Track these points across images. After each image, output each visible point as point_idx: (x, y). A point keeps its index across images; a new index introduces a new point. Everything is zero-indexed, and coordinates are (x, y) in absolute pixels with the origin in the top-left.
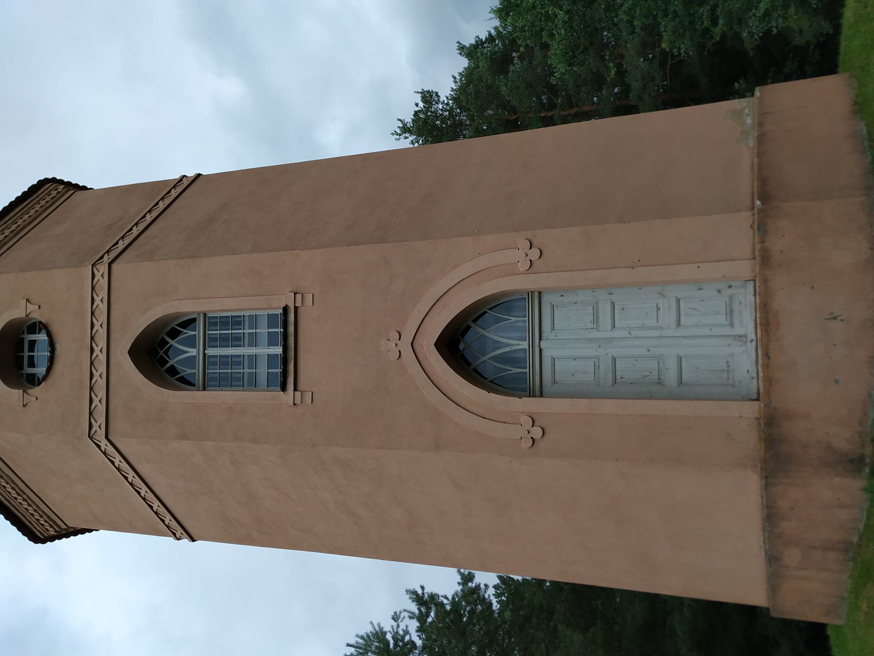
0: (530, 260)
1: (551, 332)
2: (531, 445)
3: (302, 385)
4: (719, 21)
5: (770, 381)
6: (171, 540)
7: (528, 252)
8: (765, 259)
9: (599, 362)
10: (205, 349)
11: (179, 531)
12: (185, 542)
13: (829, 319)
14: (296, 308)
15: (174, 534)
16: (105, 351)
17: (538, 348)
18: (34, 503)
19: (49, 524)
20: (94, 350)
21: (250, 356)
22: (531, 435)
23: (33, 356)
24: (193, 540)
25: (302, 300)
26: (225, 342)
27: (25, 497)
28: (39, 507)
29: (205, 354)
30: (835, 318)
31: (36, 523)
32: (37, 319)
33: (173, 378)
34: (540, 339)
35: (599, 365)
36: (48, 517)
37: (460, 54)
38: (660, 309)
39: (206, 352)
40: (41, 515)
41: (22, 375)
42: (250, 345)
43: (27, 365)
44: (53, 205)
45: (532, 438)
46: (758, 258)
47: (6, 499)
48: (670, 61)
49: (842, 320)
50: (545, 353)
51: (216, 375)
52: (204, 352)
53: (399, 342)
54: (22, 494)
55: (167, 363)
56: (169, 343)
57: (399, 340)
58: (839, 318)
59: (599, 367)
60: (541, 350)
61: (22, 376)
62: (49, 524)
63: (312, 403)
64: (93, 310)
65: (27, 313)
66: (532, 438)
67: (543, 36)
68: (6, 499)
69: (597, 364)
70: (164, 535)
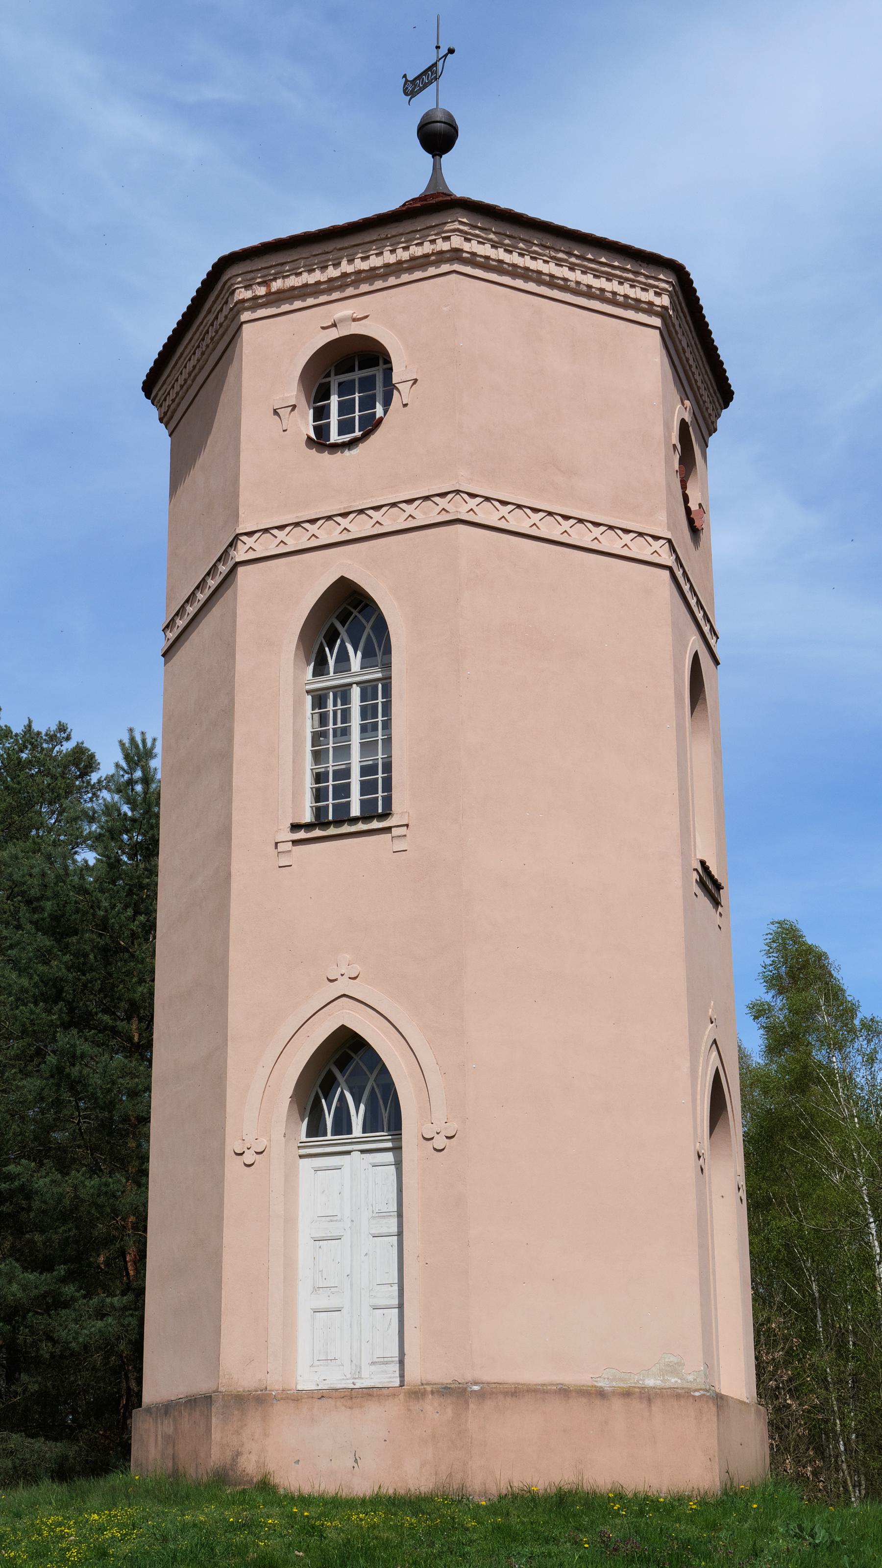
0: (433, 1138)
2: (236, 1152)
5: (298, 1400)
7: (442, 1134)
8: (417, 1394)
9: (336, 1221)
10: (357, 683)
13: (355, 1455)
14: (388, 830)
17: (351, 1149)
18: (186, 393)
20: (346, 518)
21: (348, 785)
22: (247, 1151)
23: (334, 771)
25: (400, 836)
26: (343, 791)
27: (189, 382)
28: (183, 398)
29: (351, 684)
30: (356, 1461)
31: (166, 391)
33: (360, 379)
34: (363, 1151)
35: (334, 1221)
36: (175, 411)
38: (391, 1286)
39: (354, 686)
40: (174, 401)
41: (328, 375)
42: (348, 795)
43: (341, 380)
45: (244, 1152)
46: (187, 614)
47: (182, 354)
48: (357, 1062)
49: (354, 1467)
50: (346, 1157)
51: (339, 712)
52: (354, 683)
53: (346, 977)
54: (192, 377)
55: (338, 616)
57: (350, 978)
58: (356, 1465)
59: (331, 1221)
60: (348, 1153)
61: (325, 377)
63: (280, 867)
64: (399, 505)
66: (244, 1152)
68: (182, 354)
69: (335, 1218)
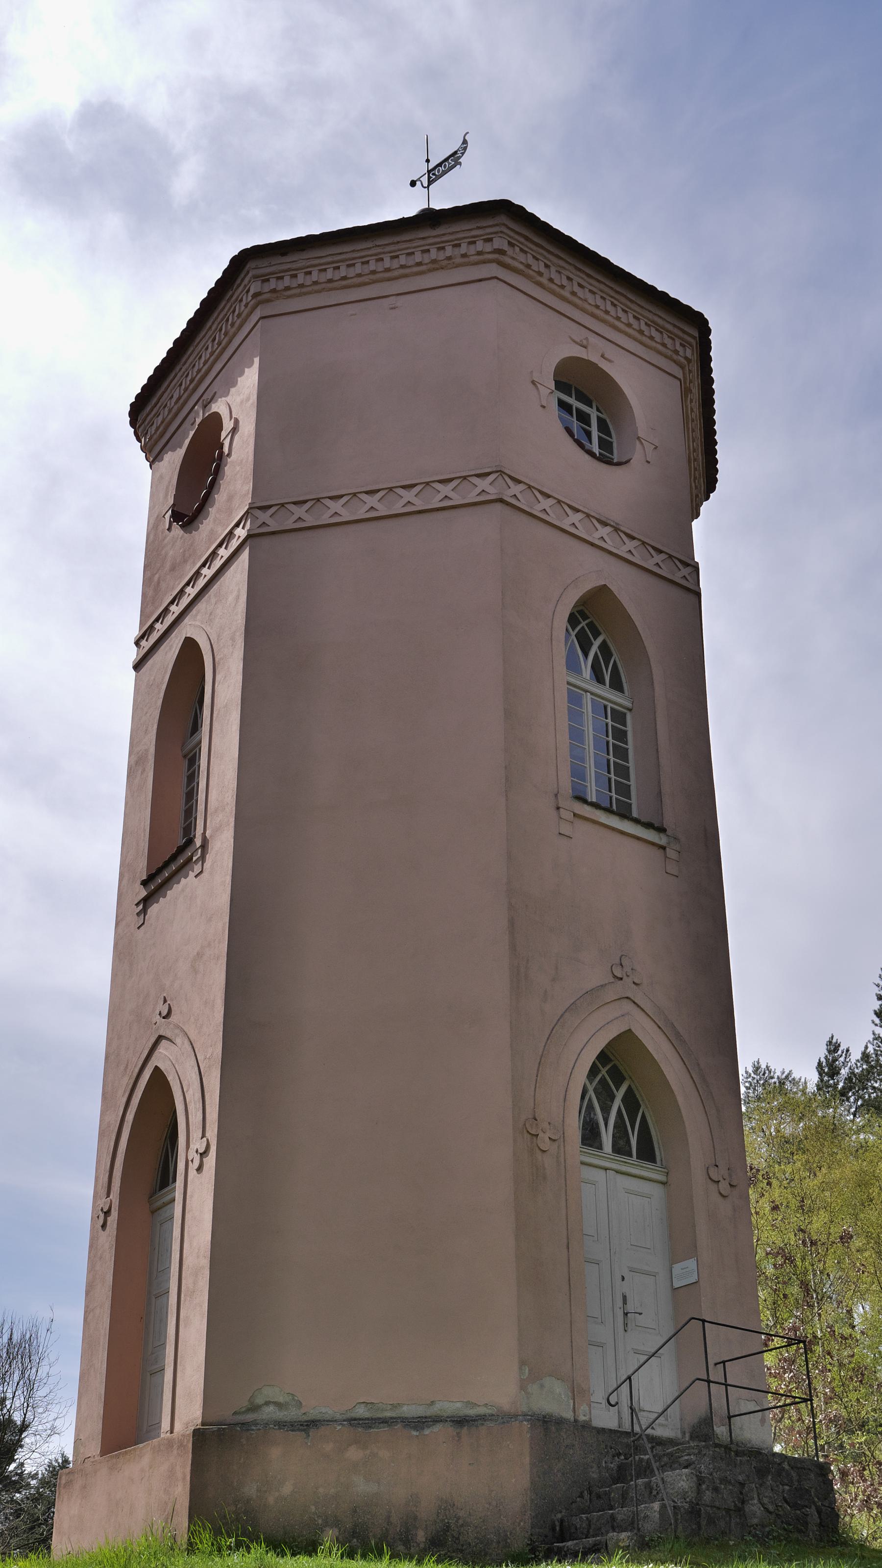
1: (624, 1188)
3: (580, 825)
4: (242, 373)
6: (135, 632)
10: (592, 694)
11: (146, 645)
12: (132, 654)
15: (142, 637)
16: (572, 530)
19: (209, 358)
24: (137, 667)
32: (560, 418)
34: (617, 1172)
37: (816, 1068)
44: (590, 275)
56: (584, 621)
62: (209, 358)
65: (539, 385)
67: (759, 1304)
70: (147, 601)
